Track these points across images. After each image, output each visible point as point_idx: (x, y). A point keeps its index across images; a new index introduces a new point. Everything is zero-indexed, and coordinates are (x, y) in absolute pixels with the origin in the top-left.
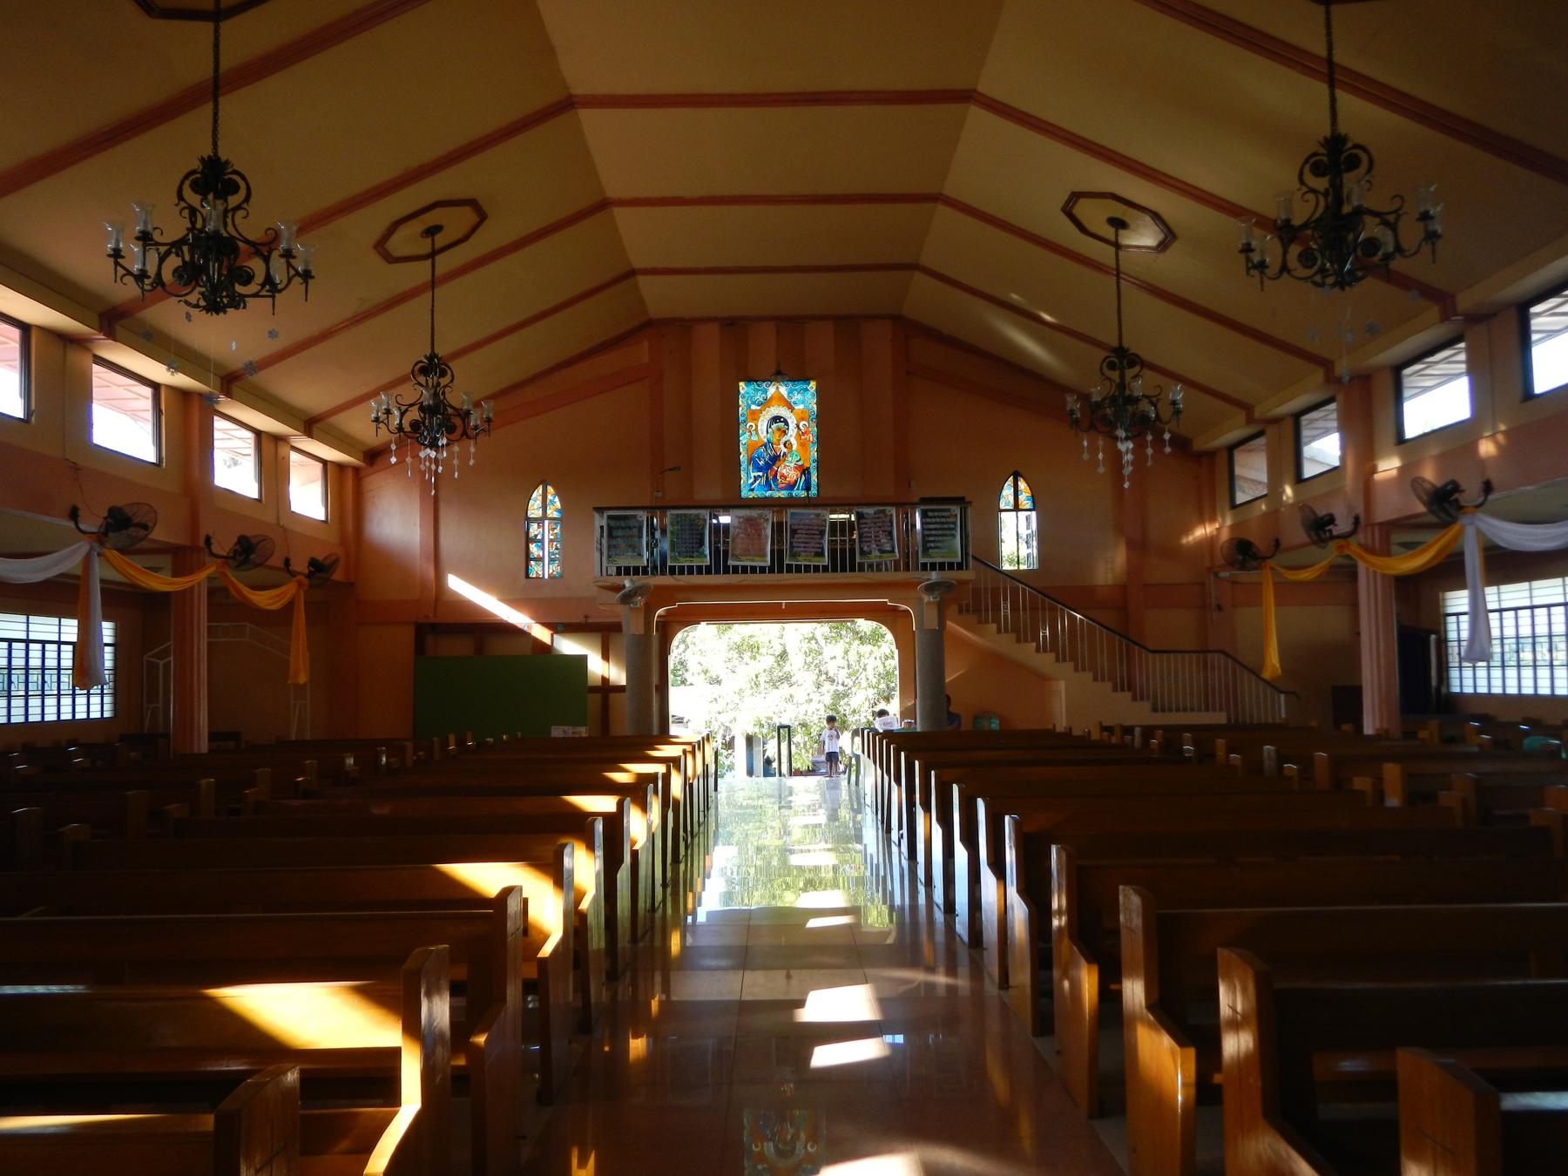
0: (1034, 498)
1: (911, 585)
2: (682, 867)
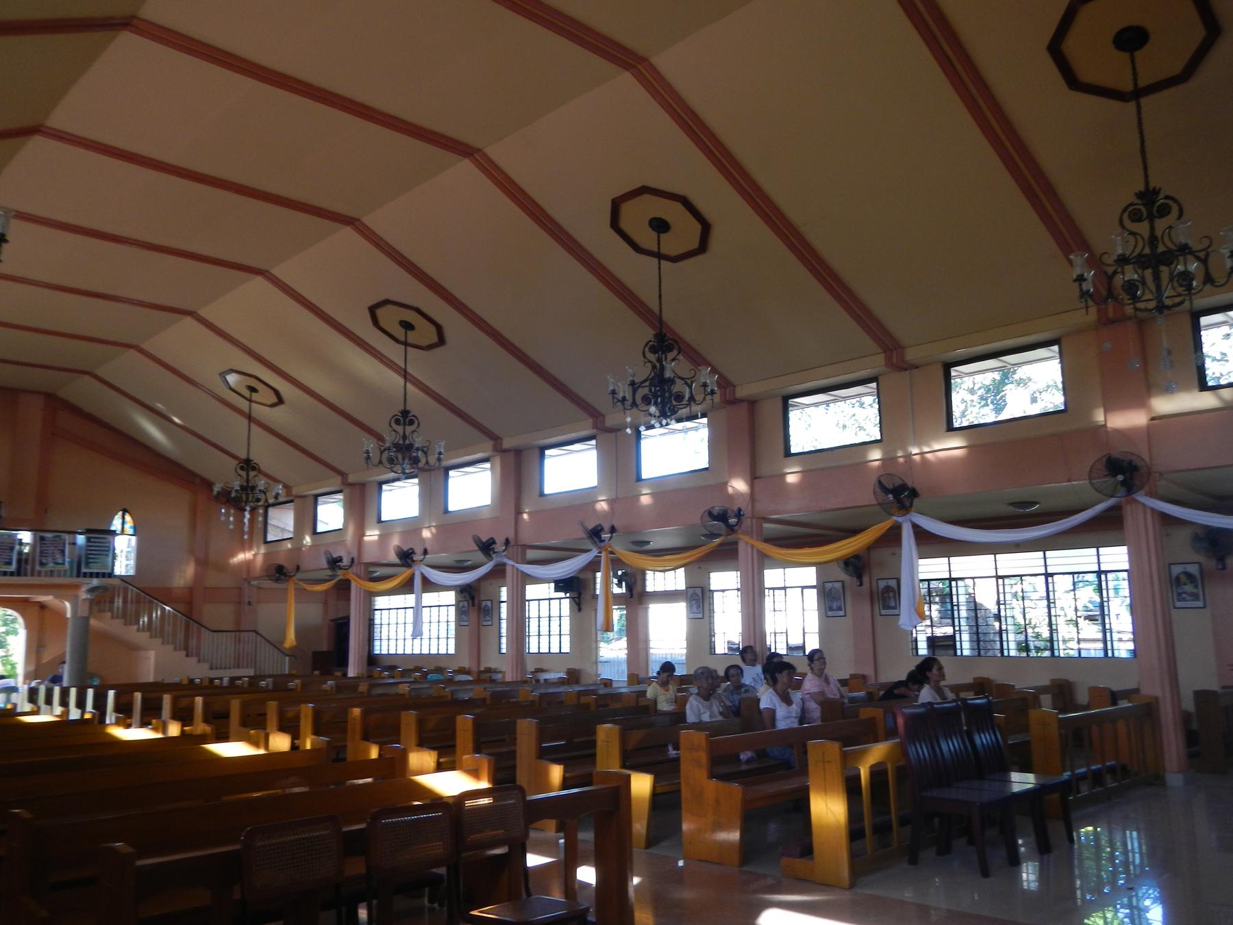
0: (135, 528)
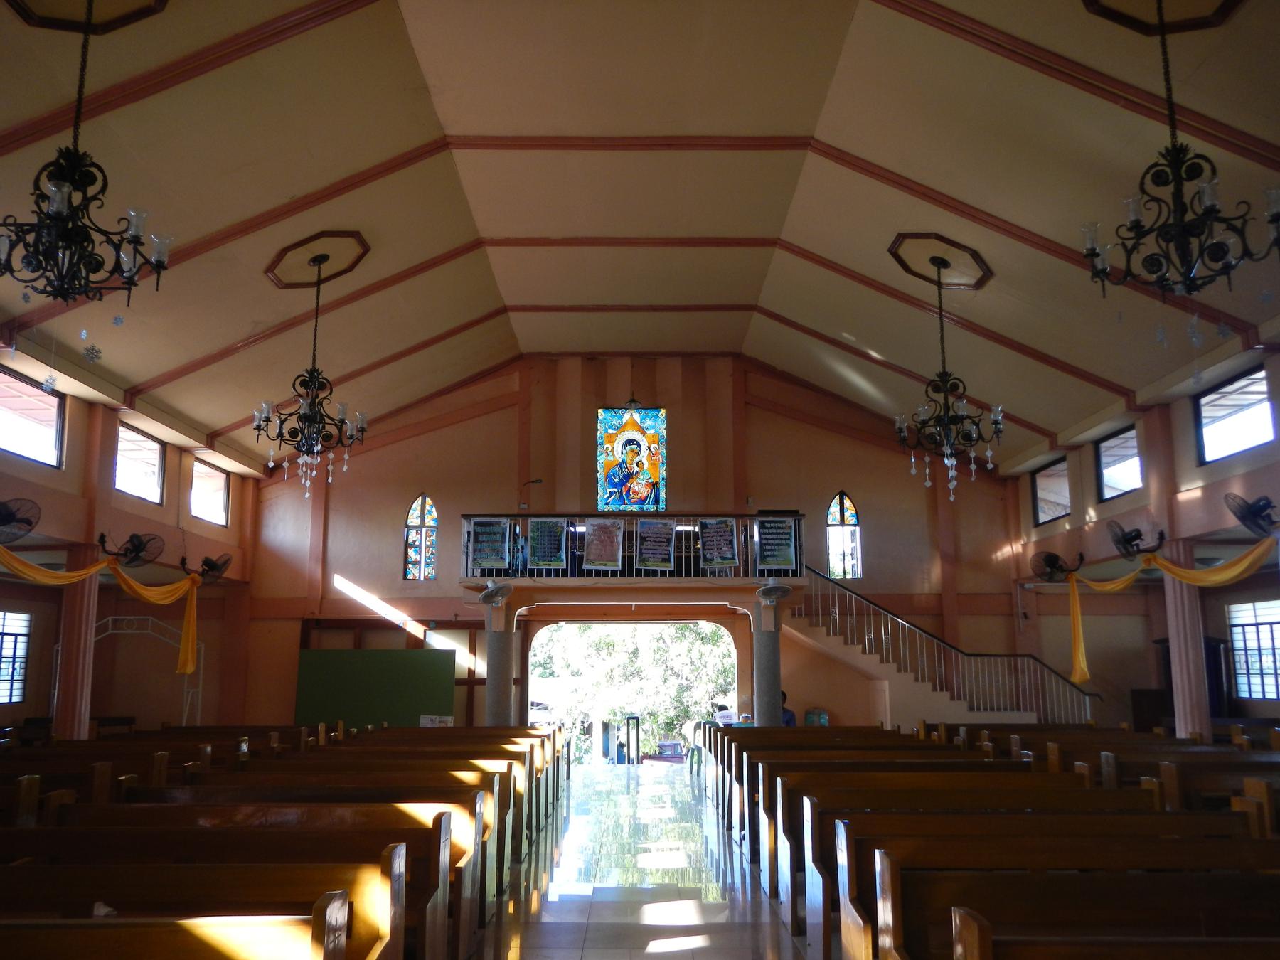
0: (857, 515)
1: (751, 590)
2: (524, 866)
